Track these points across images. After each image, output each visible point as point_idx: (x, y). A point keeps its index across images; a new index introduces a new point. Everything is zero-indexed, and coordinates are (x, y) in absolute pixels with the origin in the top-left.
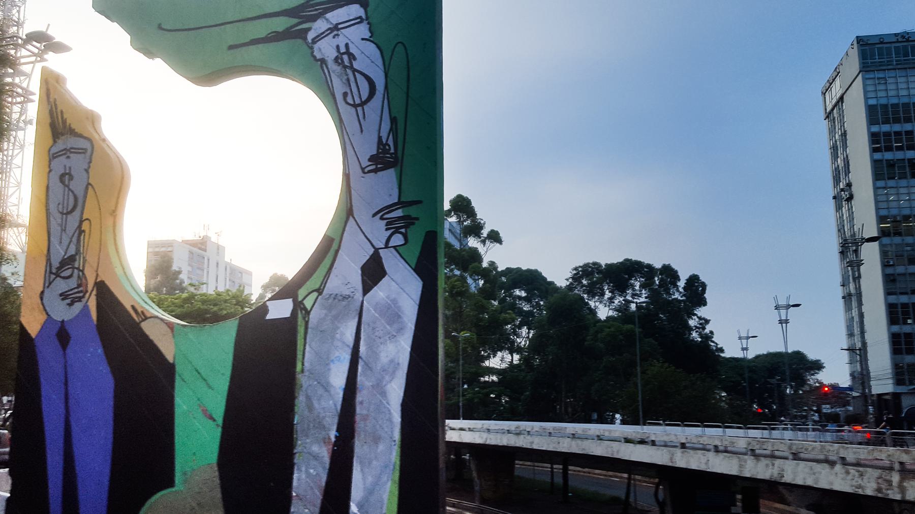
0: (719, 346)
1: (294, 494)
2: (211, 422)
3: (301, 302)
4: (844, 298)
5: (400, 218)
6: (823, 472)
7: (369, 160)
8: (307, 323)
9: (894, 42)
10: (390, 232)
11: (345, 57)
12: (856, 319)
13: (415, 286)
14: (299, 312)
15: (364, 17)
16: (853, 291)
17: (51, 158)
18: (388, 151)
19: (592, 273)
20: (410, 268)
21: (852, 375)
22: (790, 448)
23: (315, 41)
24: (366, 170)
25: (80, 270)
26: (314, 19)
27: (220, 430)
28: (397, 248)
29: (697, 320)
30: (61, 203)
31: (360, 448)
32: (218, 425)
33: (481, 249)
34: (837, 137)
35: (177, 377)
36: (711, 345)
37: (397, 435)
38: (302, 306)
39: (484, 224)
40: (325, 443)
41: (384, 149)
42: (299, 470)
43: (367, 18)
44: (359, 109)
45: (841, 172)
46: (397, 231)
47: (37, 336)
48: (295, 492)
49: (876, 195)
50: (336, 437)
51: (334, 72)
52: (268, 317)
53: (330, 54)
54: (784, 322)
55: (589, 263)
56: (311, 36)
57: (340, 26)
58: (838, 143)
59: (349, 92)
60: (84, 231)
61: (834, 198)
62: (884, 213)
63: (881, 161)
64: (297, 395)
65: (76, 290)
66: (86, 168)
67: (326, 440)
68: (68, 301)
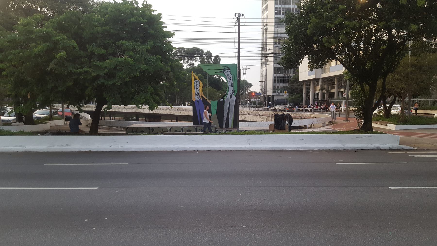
0: (223, 80)
6: (255, 118)
12: (264, 71)
13: (235, 98)
19: (181, 51)
21: (261, 89)
22: (248, 112)
26: (225, 71)
34: (265, 6)
45: (265, 19)
55: (180, 47)
56: (224, 72)
58: (265, 8)
62: (276, 36)
63: (277, 18)
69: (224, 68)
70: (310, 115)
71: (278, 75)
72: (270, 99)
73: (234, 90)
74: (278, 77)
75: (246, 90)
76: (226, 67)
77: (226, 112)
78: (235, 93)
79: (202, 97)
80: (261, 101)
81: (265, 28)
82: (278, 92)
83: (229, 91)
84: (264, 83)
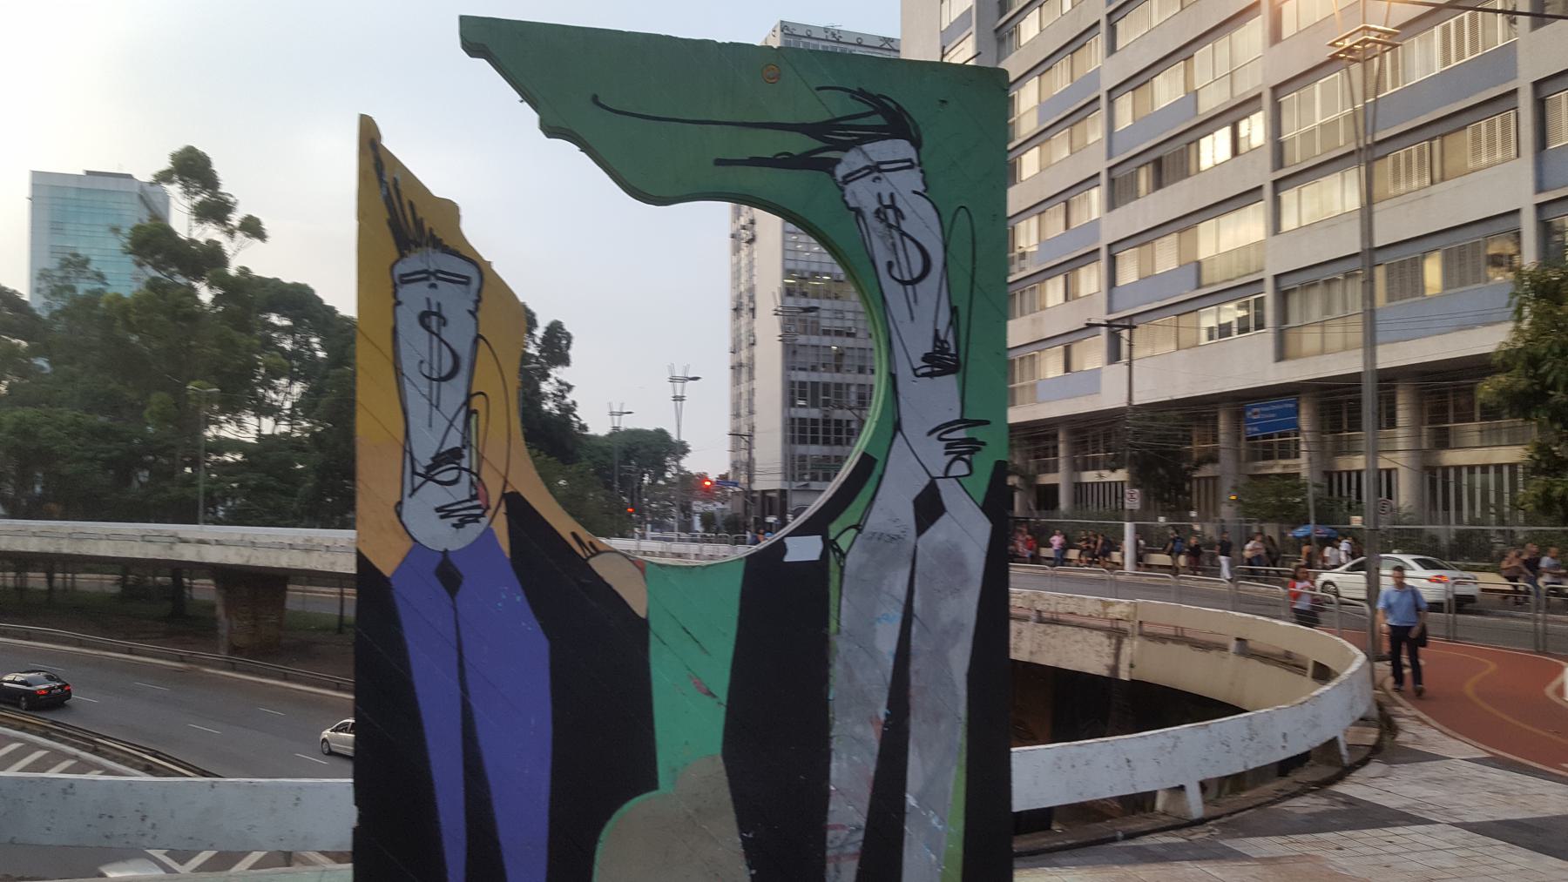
0: (582, 422)
1: (832, 788)
2: (708, 699)
3: (834, 541)
4: (733, 368)
5: (963, 441)
7: (924, 359)
8: (842, 569)
9: (823, 40)
10: (951, 457)
11: (890, 212)
12: (745, 396)
14: (831, 554)
15: (915, 161)
16: (744, 361)
17: (397, 282)
18: (945, 351)
20: (976, 507)
23: (848, 179)
24: (919, 372)
25: (472, 473)
26: (845, 147)
27: (723, 709)
28: (960, 479)
29: (557, 384)
30: (427, 358)
31: (917, 727)
32: (720, 703)
33: (228, 246)
35: (652, 638)
36: (572, 421)
37: (962, 711)
38: (835, 546)
39: (235, 203)
40: (872, 722)
41: (942, 347)
42: (839, 758)
43: (920, 164)
44: (909, 288)
46: (959, 457)
47: (395, 573)
48: (834, 786)
49: (784, 241)
50: (887, 715)
51: (874, 230)
52: (787, 559)
53: (870, 206)
54: (678, 399)
56: (841, 171)
57: (884, 167)
59: (895, 261)
60: (476, 412)
61: (733, 236)
62: (791, 265)
64: (831, 662)
65: (469, 504)
66: (471, 309)
67: (873, 720)
68: (455, 520)
69: (838, 106)
70: (1099, 607)
71: (803, 413)
72: (770, 505)
73: (964, 422)
74: (803, 421)
75: (665, 469)
76: (861, 95)
77: (859, 730)
78: (984, 464)
79: (516, 506)
80: (736, 512)
81: (745, 235)
82: (804, 480)
83: (897, 427)
84: (743, 438)
